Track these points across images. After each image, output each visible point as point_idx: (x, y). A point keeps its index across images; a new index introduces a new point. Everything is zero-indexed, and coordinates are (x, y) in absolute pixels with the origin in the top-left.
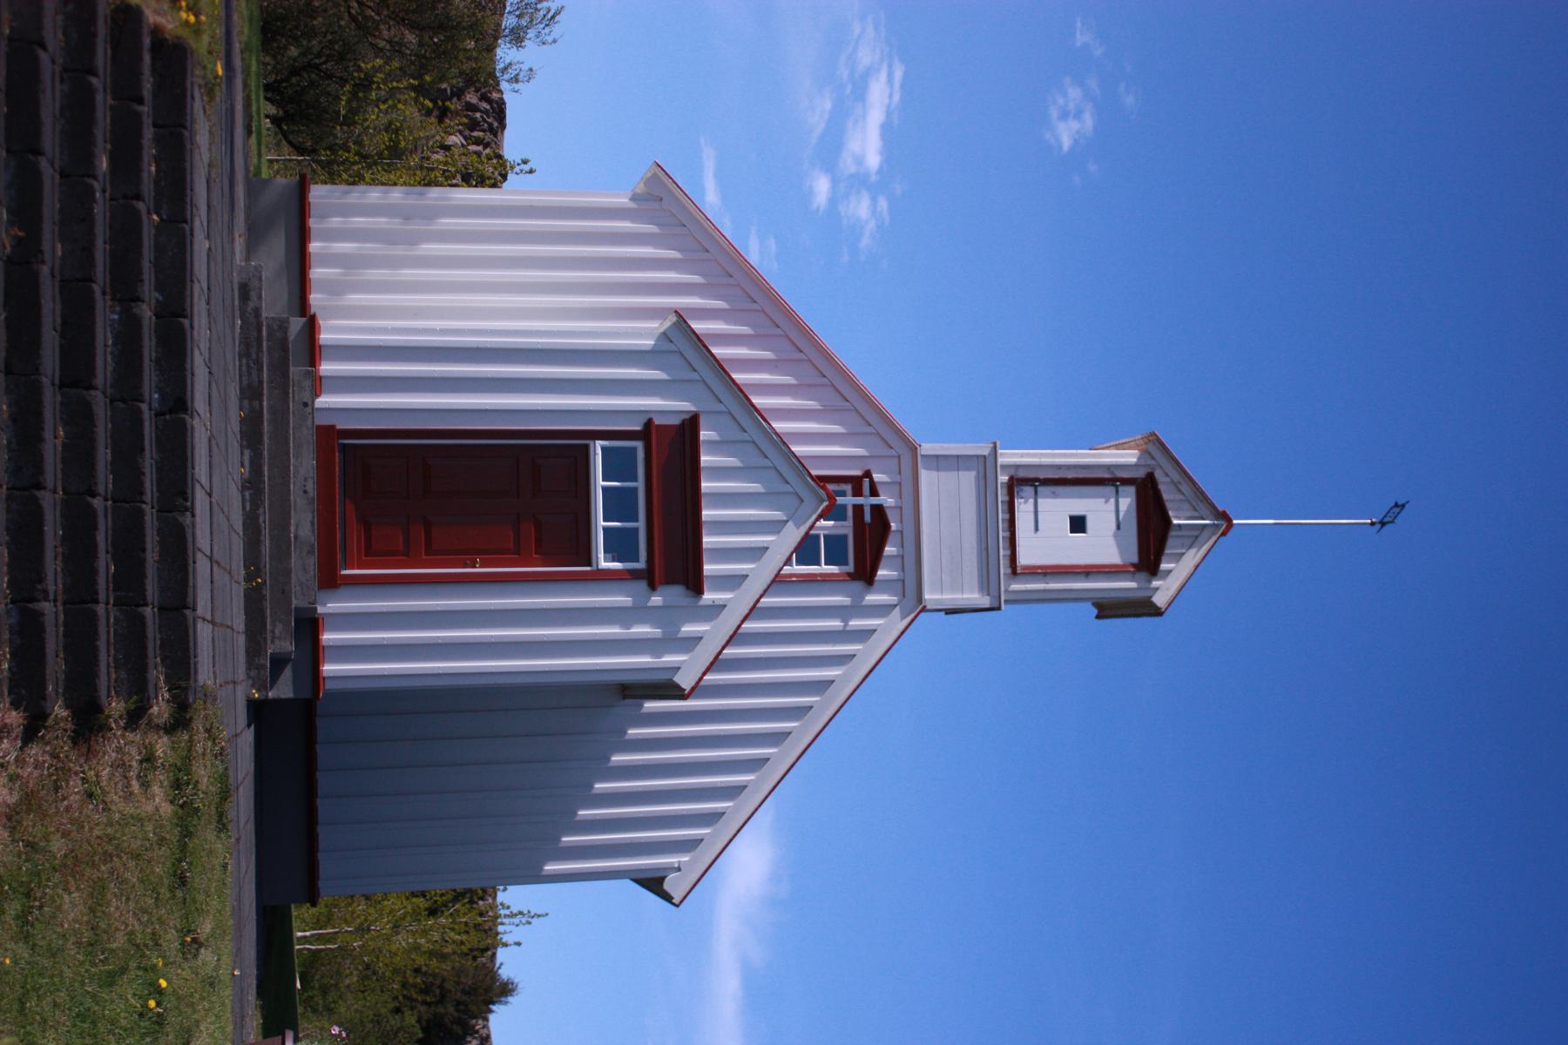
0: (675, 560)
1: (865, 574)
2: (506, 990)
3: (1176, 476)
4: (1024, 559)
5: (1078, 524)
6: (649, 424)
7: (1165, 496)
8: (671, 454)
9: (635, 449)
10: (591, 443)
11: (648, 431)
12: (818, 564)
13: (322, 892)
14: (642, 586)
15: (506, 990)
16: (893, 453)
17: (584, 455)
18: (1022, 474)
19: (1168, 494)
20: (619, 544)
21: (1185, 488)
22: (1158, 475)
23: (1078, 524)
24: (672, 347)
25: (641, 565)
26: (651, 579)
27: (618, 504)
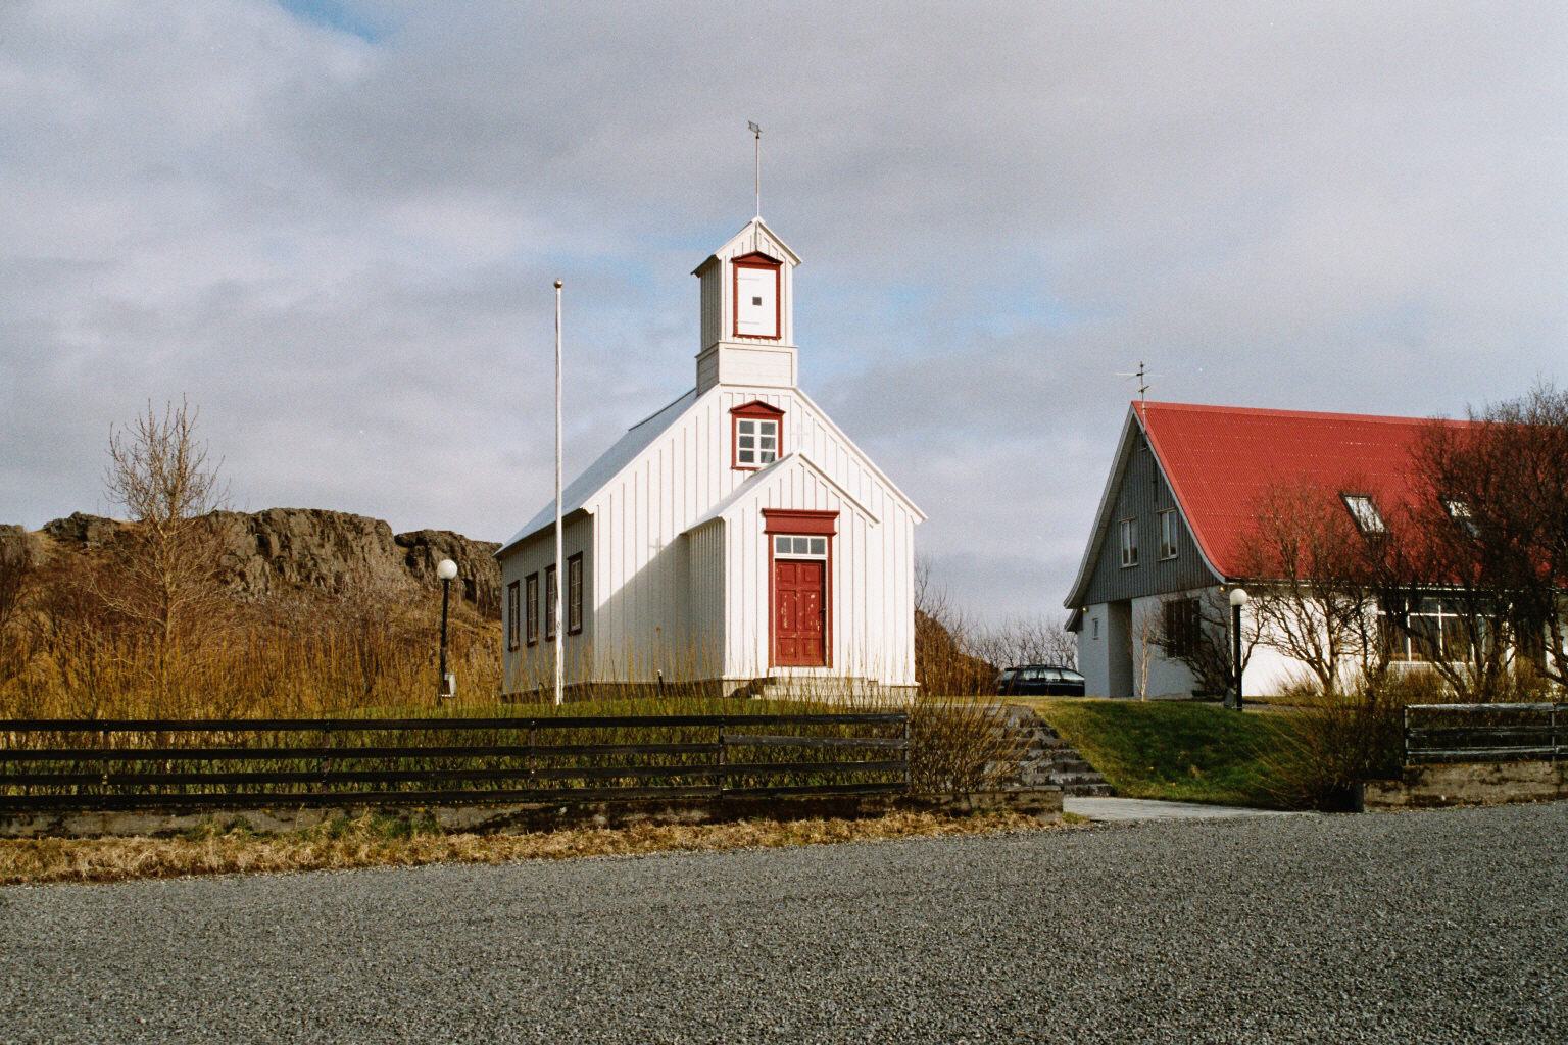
1: (777, 413)
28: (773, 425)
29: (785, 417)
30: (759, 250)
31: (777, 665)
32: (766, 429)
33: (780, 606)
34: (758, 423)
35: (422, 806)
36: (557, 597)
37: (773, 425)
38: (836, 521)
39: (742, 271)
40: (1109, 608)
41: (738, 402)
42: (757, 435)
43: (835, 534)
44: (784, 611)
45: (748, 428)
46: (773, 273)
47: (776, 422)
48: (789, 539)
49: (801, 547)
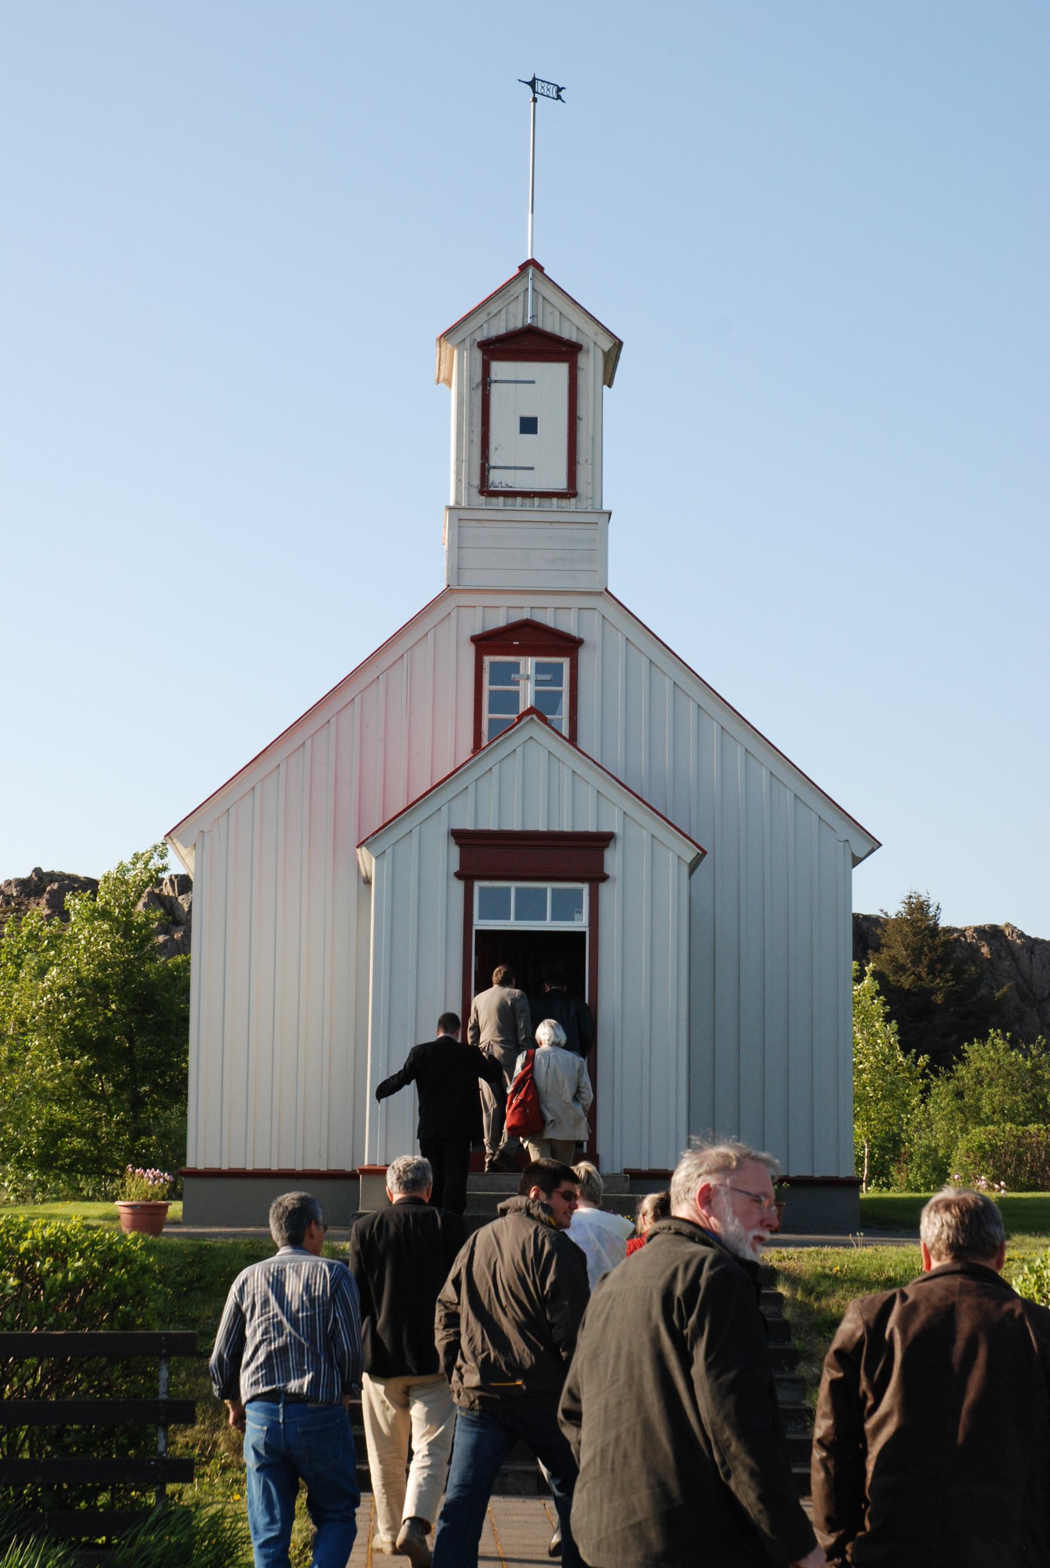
0: (578, 856)
1: (568, 645)
2: (918, 909)
3: (481, 318)
4: (560, 483)
5: (529, 425)
6: (458, 875)
7: (502, 331)
8: (486, 854)
9: (481, 889)
10: (475, 928)
11: (467, 875)
12: (560, 693)
13: (850, 1174)
14: (604, 888)
15: (918, 909)
16: (454, 614)
17: (484, 936)
18: (476, 481)
19: (499, 328)
20: (566, 907)
21: (494, 308)
22: (480, 337)
23: (529, 425)
24: (389, 852)
25: (585, 888)
26: (597, 877)
27: (531, 907)
29: (583, 654)
41: (499, 620)
43: (605, 878)
46: (562, 369)
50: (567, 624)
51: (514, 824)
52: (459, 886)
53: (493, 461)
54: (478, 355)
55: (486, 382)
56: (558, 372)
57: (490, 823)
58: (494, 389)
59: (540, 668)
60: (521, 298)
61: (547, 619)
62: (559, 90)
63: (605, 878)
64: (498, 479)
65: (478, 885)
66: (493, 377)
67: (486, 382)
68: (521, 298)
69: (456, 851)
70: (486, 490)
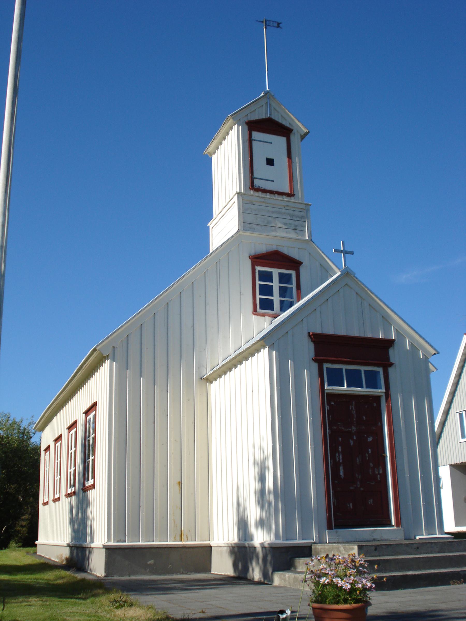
1: (295, 264)
6: (315, 360)
9: (327, 369)
10: (326, 391)
11: (319, 360)
26: (387, 364)
28: (290, 275)
29: (302, 270)
30: (273, 117)
31: (335, 528)
32: (284, 278)
33: (334, 451)
34: (276, 272)
35: (28, 508)
36: (293, 120)
37: (290, 275)
38: (391, 351)
39: (256, 135)
40: (106, 551)
41: (263, 249)
42: (276, 284)
43: (391, 364)
44: (339, 458)
45: (267, 277)
46: (283, 140)
47: (293, 273)
48: (341, 370)
49: (354, 380)
50: (294, 254)
51: (342, 331)
52: (315, 366)
53: (255, 175)
54: (246, 127)
55: (251, 141)
56: (281, 141)
57: (330, 330)
58: (254, 143)
59: (281, 275)
60: (264, 106)
61: (285, 251)
62: (279, 24)
63: (391, 364)
64: (257, 183)
65: (326, 366)
66: (253, 138)
67: (251, 141)
68: (264, 106)
69: (312, 346)
70: (253, 187)
